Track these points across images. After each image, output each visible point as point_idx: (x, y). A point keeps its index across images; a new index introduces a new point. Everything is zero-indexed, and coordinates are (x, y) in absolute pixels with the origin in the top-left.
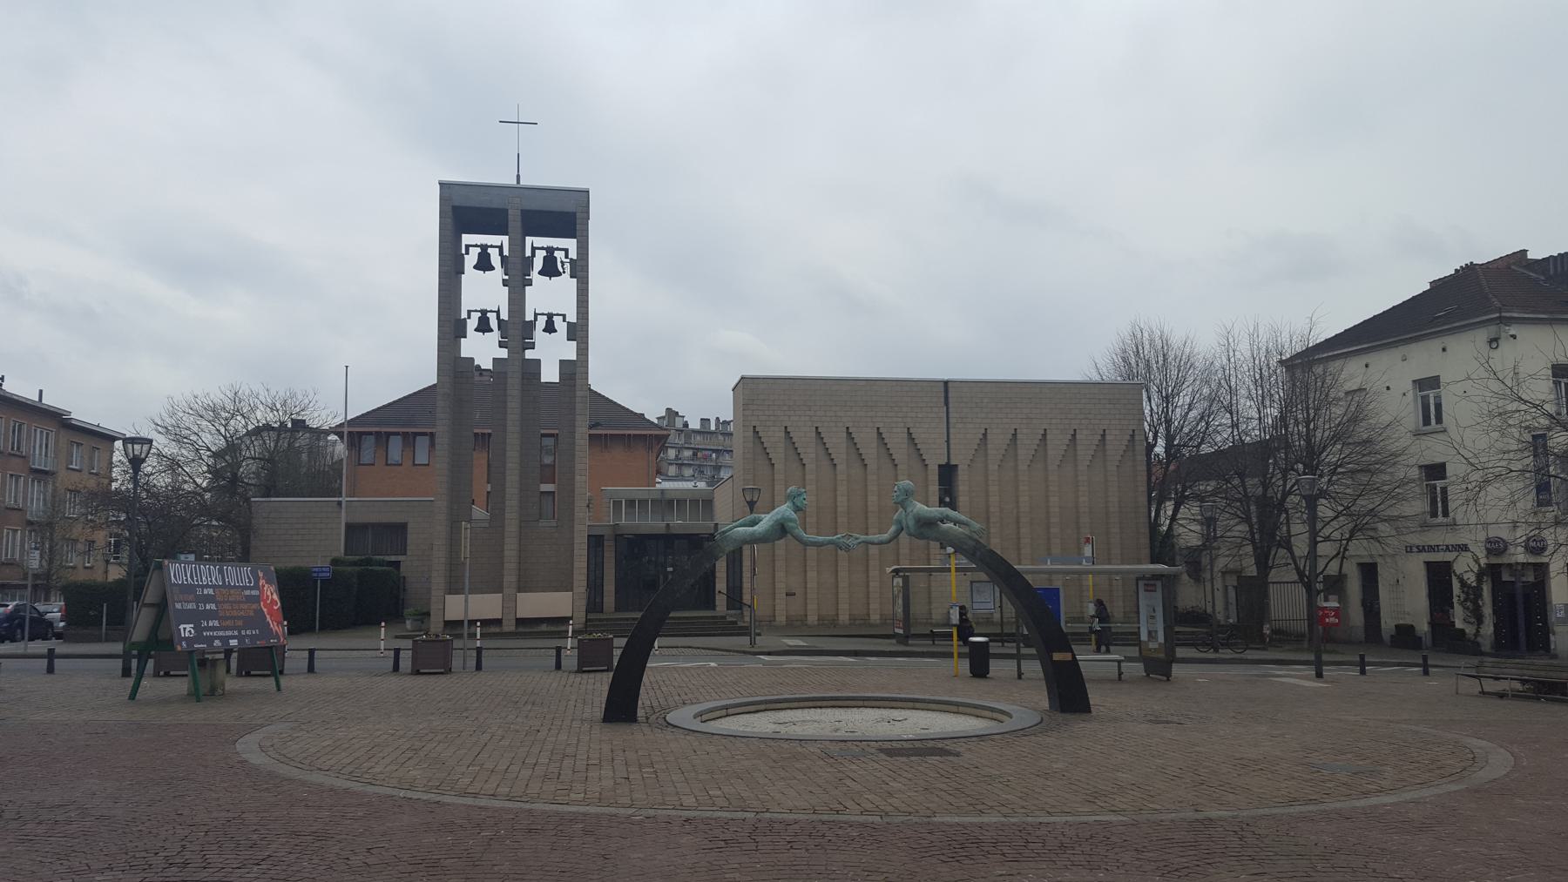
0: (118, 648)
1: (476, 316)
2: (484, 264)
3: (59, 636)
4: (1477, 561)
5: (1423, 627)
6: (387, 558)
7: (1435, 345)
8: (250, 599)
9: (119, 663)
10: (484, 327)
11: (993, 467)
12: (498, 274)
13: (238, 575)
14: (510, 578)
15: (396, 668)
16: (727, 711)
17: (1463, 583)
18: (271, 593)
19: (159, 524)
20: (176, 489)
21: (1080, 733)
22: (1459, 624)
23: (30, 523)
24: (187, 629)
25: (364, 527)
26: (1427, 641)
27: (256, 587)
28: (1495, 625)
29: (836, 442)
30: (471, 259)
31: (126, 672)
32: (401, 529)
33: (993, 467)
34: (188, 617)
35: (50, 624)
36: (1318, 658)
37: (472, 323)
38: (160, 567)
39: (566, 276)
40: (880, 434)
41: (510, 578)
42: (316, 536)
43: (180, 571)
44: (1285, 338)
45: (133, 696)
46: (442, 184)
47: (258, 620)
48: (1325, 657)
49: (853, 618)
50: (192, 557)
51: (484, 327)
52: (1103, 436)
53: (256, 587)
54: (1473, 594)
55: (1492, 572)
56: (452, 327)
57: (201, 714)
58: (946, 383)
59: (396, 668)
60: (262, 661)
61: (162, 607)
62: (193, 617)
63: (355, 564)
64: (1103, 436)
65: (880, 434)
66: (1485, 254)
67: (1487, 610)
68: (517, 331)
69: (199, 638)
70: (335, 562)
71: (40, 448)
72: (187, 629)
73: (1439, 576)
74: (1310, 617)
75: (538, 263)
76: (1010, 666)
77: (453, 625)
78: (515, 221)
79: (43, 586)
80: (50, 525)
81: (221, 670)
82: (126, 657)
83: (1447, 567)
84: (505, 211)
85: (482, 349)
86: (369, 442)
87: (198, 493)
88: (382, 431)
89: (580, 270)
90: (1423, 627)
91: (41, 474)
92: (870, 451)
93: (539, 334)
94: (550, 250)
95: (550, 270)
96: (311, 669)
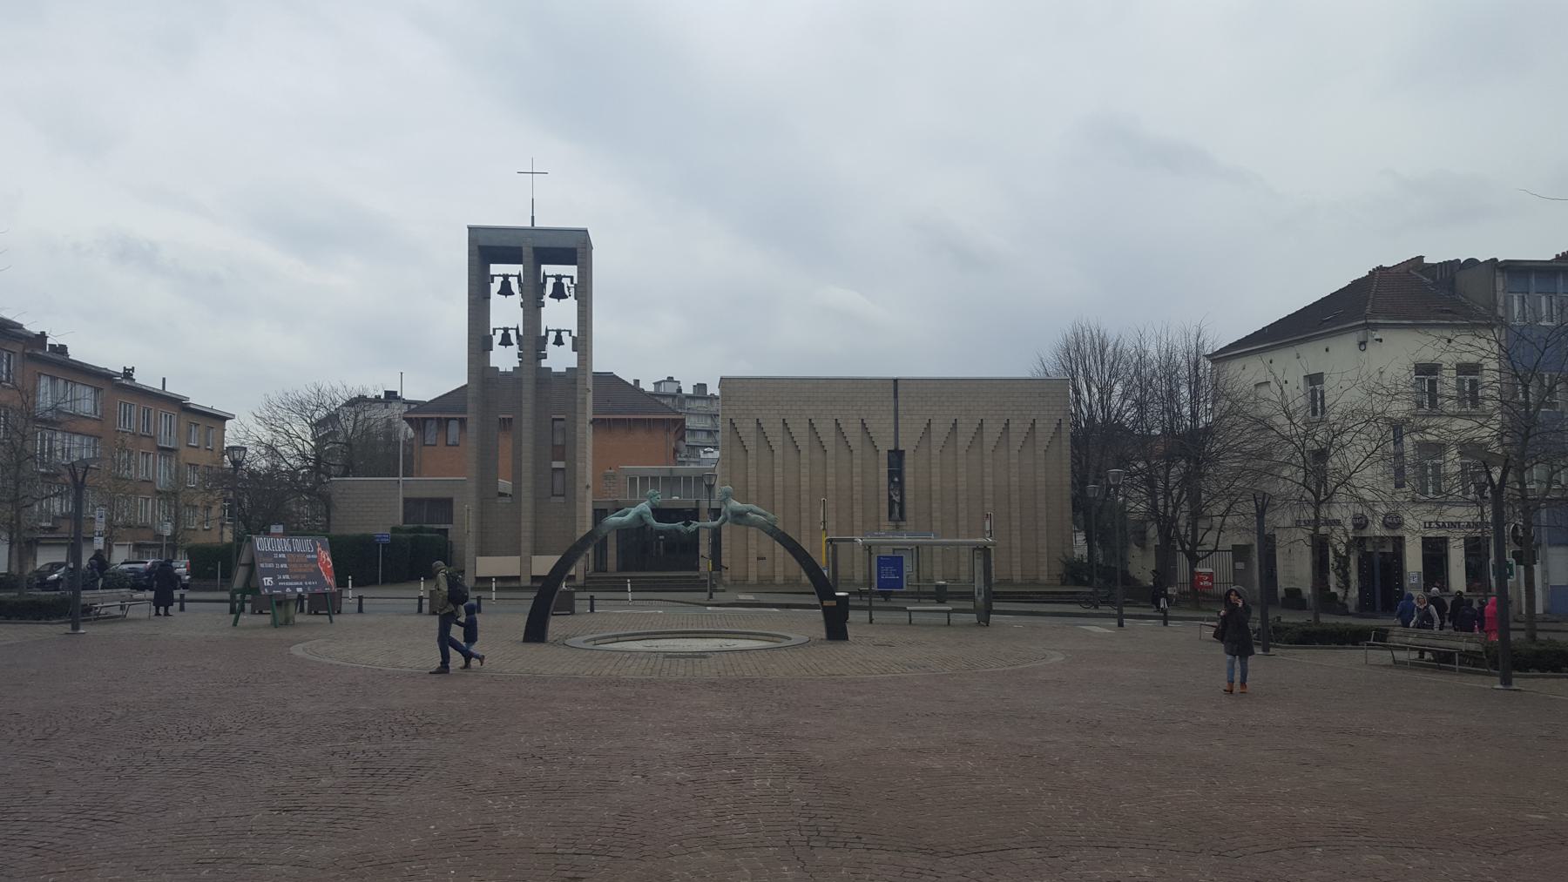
0: (226, 595)
1: (500, 333)
2: (506, 290)
3: (185, 587)
4: (1346, 535)
5: (1307, 590)
6: (437, 526)
7: (1320, 345)
8: (311, 561)
9: (228, 606)
10: (506, 341)
11: (935, 452)
12: (517, 298)
13: (302, 545)
14: (526, 545)
15: (420, 610)
16: (618, 638)
17: (1336, 552)
18: (325, 556)
19: (260, 497)
20: (275, 467)
21: (837, 649)
22: (1333, 589)
23: (158, 492)
24: (268, 581)
25: (419, 502)
26: (1311, 602)
27: (315, 552)
28: (1360, 590)
29: (800, 431)
30: (496, 286)
31: (232, 611)
32: (448, 502)
33: (935, 452)
34: (268, 573)
35: (179, 577)
36: (1121, 611)
37: (497, 339)
38: (250, 540)
39: (572, 298)
40: (838, 424)
41: (526, 545)
42: (376, 508)
43: (262, 543)
44: (1152, 351)
45: (235, 624)
46: (470, 228)
47: (317, 575)
48: (1126, 611)
49: (787, 579)
50: (280, 529)
51: (506, 341)
52: (1033, 424)
53: (315, 552)
54: (1343, 562)
55: (1360, 542)
56: (480, 341)
57: (274, 634)
58: (896, 380)
59: (420, 610)
60: (324, 604)
61: (252, 566)
62: (273, 573)
63: (410, 531)
64: (1033, 424)
65: (838, 424)
66: (1392, 258)
67: (1354, 576)
68: (533, 341)
69: (276, 586)
70: (394, 530)
71: (166, 429)
72: (268, 581)
73: (1320, 546)
74: (1192, 579)
75: (549, 289)
76: (865, 615)
77: (485, 581)
78: (527, 253)
79: (173, 545)
80: (175, 494)
81: (292, 607)
82: (232, 601)
83: (1326, 537)
84: (520, 249)
85: (504, 359)
86: (432, 427)
87: (294, 472)
88: (433, 418)
89: (584, 294)
90: (1307, 590)
91: (167, 451)
92: (829, 438)
93: (550, 347)
94: (559, 278)
95: (559, 293)
96: (360, 610)
